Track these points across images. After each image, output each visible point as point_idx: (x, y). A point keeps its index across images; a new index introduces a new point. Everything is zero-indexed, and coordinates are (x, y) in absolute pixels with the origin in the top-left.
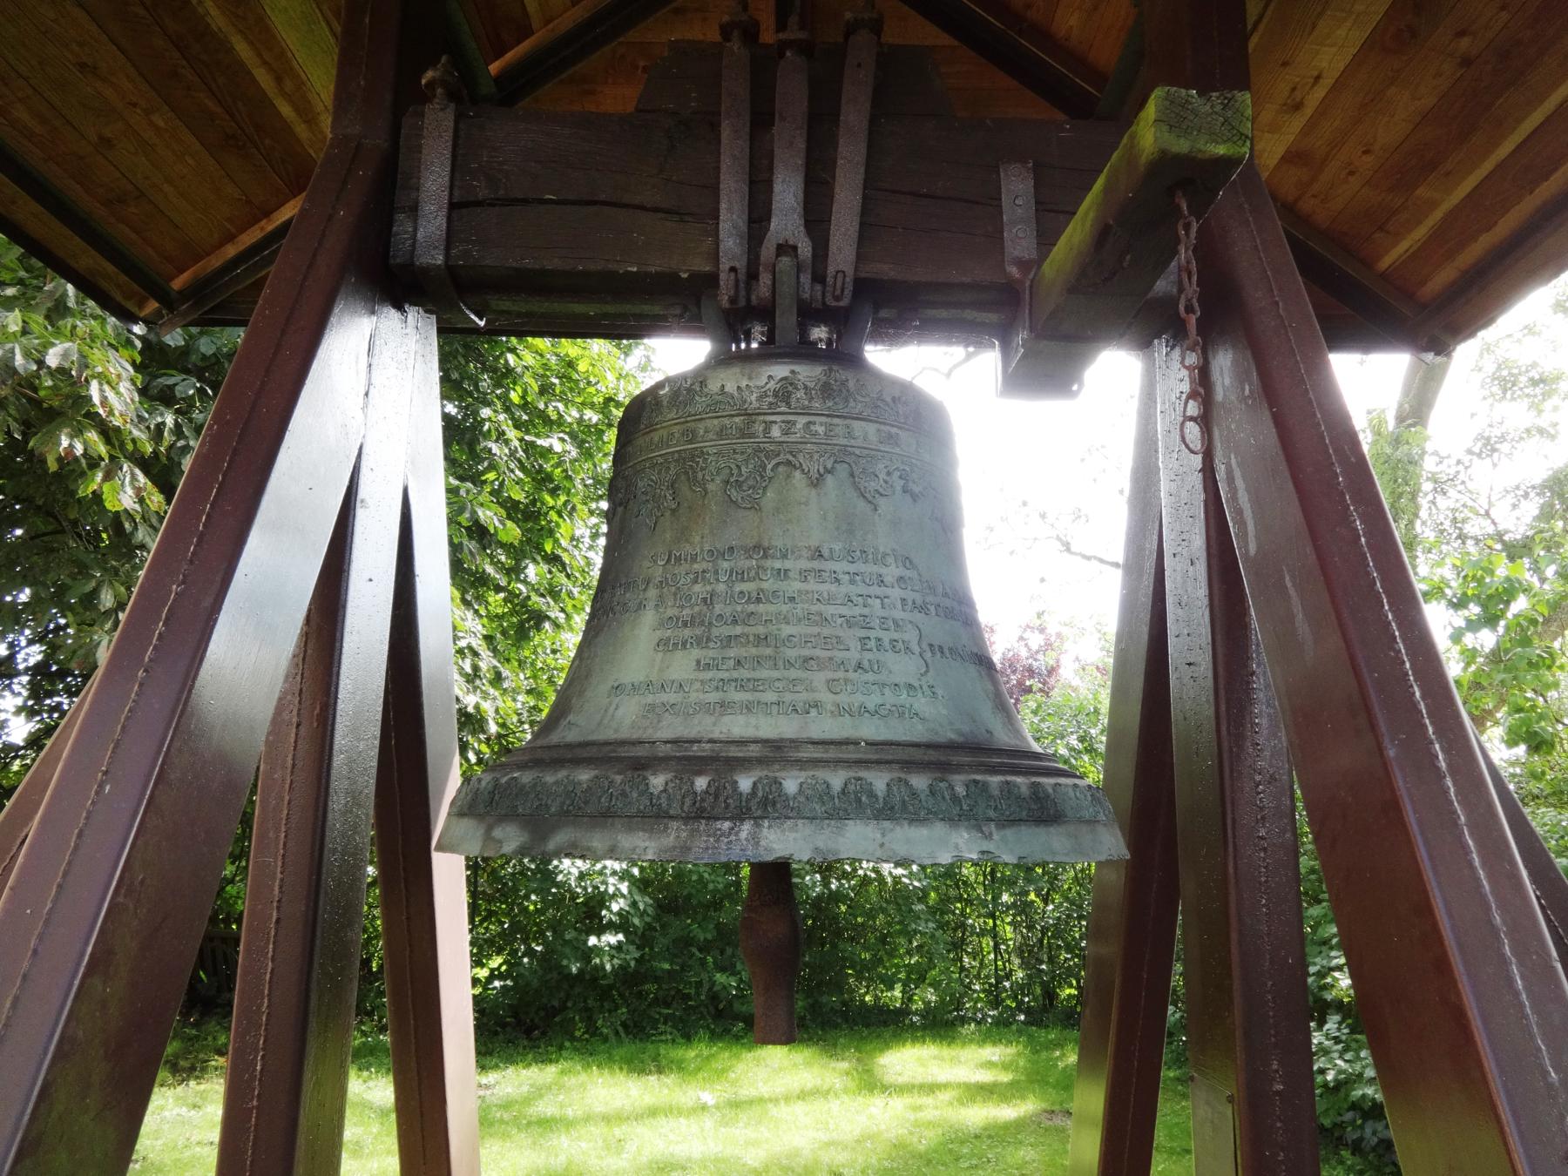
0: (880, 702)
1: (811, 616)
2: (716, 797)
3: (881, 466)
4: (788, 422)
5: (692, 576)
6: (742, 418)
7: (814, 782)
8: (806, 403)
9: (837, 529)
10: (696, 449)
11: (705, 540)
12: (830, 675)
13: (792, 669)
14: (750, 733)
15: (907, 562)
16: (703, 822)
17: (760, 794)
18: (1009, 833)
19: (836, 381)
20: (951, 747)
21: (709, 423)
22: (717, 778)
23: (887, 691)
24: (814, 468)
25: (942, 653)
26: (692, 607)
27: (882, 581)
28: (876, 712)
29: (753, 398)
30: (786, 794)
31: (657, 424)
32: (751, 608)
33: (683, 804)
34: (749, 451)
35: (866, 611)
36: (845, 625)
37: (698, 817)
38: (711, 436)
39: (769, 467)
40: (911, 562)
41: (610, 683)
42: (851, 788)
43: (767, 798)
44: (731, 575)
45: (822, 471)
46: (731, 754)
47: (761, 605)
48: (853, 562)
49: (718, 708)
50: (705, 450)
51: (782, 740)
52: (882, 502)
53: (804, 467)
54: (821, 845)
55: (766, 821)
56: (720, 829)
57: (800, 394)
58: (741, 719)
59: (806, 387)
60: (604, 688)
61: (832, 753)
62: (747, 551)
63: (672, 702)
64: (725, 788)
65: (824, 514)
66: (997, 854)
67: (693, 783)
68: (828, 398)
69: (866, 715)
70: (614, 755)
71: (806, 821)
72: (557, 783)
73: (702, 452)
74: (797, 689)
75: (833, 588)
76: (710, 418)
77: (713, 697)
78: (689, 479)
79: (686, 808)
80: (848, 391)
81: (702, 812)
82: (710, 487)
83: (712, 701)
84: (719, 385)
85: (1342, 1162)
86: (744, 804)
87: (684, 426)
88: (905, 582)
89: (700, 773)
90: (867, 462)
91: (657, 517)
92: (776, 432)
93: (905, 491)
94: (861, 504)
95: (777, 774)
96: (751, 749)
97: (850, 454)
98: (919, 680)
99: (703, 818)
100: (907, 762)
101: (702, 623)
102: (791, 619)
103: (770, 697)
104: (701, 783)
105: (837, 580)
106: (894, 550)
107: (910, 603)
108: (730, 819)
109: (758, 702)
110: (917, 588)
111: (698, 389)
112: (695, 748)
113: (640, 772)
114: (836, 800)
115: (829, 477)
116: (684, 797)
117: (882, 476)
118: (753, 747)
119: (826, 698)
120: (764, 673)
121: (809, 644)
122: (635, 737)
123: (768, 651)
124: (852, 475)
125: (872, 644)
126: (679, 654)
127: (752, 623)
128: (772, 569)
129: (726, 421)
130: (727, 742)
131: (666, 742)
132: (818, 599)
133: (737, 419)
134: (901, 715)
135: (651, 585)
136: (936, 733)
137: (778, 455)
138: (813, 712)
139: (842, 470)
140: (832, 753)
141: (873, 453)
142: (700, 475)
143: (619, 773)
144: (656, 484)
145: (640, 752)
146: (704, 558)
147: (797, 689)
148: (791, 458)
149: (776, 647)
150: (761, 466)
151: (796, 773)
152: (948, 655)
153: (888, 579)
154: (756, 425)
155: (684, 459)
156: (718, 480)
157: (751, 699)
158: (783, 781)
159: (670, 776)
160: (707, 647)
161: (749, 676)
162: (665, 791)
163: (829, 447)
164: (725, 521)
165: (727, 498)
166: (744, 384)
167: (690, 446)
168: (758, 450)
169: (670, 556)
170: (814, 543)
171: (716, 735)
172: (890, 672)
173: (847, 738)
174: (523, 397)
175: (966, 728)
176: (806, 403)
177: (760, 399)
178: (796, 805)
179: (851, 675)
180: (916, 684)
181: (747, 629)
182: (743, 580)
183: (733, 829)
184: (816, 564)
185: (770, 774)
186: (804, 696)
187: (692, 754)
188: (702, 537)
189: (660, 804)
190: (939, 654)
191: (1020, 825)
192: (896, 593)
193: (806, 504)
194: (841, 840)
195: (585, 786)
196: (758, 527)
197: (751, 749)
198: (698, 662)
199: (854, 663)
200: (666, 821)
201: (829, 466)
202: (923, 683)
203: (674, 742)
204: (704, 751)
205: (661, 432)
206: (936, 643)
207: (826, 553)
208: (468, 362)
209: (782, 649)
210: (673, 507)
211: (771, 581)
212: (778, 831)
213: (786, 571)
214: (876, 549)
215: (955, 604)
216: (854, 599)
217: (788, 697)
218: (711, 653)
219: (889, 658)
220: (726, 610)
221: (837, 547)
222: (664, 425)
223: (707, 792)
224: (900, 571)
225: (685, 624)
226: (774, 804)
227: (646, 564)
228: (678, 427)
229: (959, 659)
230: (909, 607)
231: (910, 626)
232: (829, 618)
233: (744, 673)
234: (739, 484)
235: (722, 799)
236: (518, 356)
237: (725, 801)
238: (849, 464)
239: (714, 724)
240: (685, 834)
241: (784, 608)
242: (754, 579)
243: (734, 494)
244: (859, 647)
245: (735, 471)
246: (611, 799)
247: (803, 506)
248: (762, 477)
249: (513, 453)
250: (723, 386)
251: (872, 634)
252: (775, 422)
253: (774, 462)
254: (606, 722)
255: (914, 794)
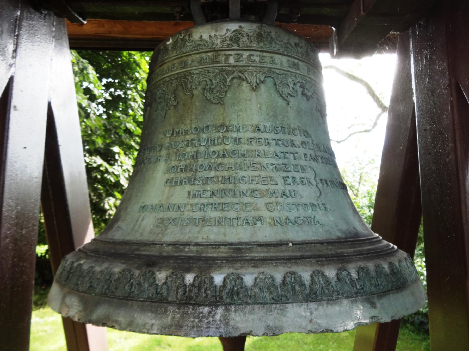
0: (297, 216)
1: (255, 165)
2: (199, 289)
3: (290, 80)
4: (239, 55)
5: (185, 143)
6: (212, 53)
7: (264, 277)
8: (248, 44)
9: (268, 114)
10: (187, 71)
11: (193, 122)
12: (268, 200)
13: (245, 197)
14: (221, 238)
15: (306, 134)
16: (191, 307)
17: (229, 287)
18: (384, 301)
19: (264, 32)
20: (339, 242)
21: (194, 57)
22: (199, 275)
23: (300, 208)
24: (254, 80)
25: (327, 184)
26: (185, 160)
27: (293, 144)
28: (296, 222)
29: (219, 41)
30: (246, 286)
31: (165, 60)
32: (220, 160)
33: (177, 293)
34: (217, 71)
35: (285, 161)
36: (274, 170)
37: (187, 304)
38: (195, 64)
39: (228, 80)
40: (308, 133)
41: (141, 204)
42: (288, 280)
43: (233, 290)
44: (208, 142)
45: (258, 82)
46: (209, 255)
47: (225, 159)
48: (277, 133)
49: (201, 222)
50: (191, 72)
51: (240, 243)
52: (291, 100)
53: (248, 79)
54: (271, 323)
55: (233, 307)
56: (202, 313)
57: (245, 39)
58: (215, 229)
59: (248, 35)
60: (136, 207)
61: (272, 253)
62: (216, 127)
63: (174, 217)
64: (205, 282)
65: (260, 106)
66: (380, 317)
67: (184, 279)
68: (260, 41)
69: (290, 224)
70: (137, 252)
71: (260, 306)
72: (101, 272)
73: (190, 73)
74: (248, 209)
75: (267, 148)
76: (194, 54)
77: (198, 215)
78: (183, 89)
79: (179, 296)
80: (272, 38)
81: (190, 300)
82: (195, 92)
83: (197, 217)
84: (199, 36)
85: (407, 327)
86: (218, 293)
87: (180, 60)
88: (305, 144)
89: (188, 270)
90: (283, 77)
91: (166, 111)
92: (232, 61)
93: (303, 94)
94: (280, 101)
95: (239, 271)
96: (221, 250)
97: (274, 72)
98: (317, 200)
99: (191, 304)
100: (320, 256)
101: (191, 170)
102: (243, 166)
103: (232, 214)
104: (189, 278)
105: (269, 144)
106: (299, 127)
107: (309, 156)
108: (209, 305)
109: (225, 218)
110: (311, 148)
111: (187, 39)
112: (186, 250)
113: (150, 269)
114: (279, 290)
115: (262, 86)
116: (178, 289)
117: (291, 85)
118: (223, 249)
119: (265, 214)
120: (229, 200)
121: (254, 182)
122: (151, 239)
123: (231, 186)
124: (275, 85)
125: (290, 180)
126: (178, 188)
127: (220, 169)
128: (231, 138)
129: (204, 55)
130: (207, 245)
131: (169, 245)
132: (258, 155)
133: (210, 54)
134: (310, 223)
135: (163, 148)
136: (330, 233)
137: (233, 73)
138: (259, 224)
139: (269, 82)
140: (272, 253)
141: (286, 72)
142: (189, 86)
143: (138, 268)
144: (165, 92)
145: (153, 251)
146: (192, 133)
147: (248, 209)
148: (241, 75)
149: (235, 184)
150: (223, 79)
151: (251, 270)
152: (330, 185)
153: (297, 143)
154: (220, 57)
155: (180, 77)
156: (199, 88)
157: (221, 216)
158: (243, 277)
159: (169, 272)
160: (194, 184)
161: (219, 202)
162: (165, 283)
163: (262, 69)
164: (204, 111)
165: (204, 98)
166: (213, 34)
167: (183, 70)
168: (221, 71)
169: (173, 132)
170: (255, 122)
171: (200, 240)
172: (301, 197)
173: (280, 241)
174: (142, 88)
175: (344, 227)
176: (248, 44)
177: (222, 42)
178: (253, 294)
179: (280, 200)
180: (316, 203)
181: (218, 173)
182: (214, 144)
183: (210, 312)
184: (256, 135)
185: (235, 272)
186: (253, 213)
187: (184, 254)
188: (191, 121)
189: (162, 293)
190: (325, 185)
191: (389, 294)
192: (301, 151)
193: (250, 100)
194: (284, 319)
195: (117, 276)
196: (223, 114)
197: (221, 250)
198: (189, 193)
199: (280, 192)
200: (166, 305)
201: (262, 79)
202: (319, 202)
203: (173, 244)
204: (192, 252)
205: (168, 64)
206: (323, 178)
207: (262, 128)
208: (123, 76)
209: (238, 185)
210: (175, 104)
211: (230, 145)
212: (242, 314)
213: (239, 139)
214: (290, 126)
215: (329, 156)
216: (279, 154)
217: (243, 215)
218: (197, 188)
219: (300, 188)
220: (205, 162)
221: (268, 124)
222: (170, 60)
223: (192, 285)
224: (303, 139)
225: (182, 170)
226: (238, 294)
227: (161, 136)
228: (177, 60)
229: (335, 186)
230: (308, 159)
231: (309, 169)
232: (265, 166)
233: (216, 200)
234: (211, 90)
235: (203, 290)
236: (140, 74)
237: (205, 292)
238: (273, 78)
239: (199, 233)
240: (178, 316)
241: (239, 160)
242: (221, 144)
243: (209, 96)
244: (283, 183)
245: (209, 83)
246: (132, 287)
247: (248, 102)
248: (224, 85)
249: (139, 106)
250: (201, 36)
251: (290, 174)
252: (231, 55)
253: (231, 77)
254: (136, 228)
255: (328, 282)
